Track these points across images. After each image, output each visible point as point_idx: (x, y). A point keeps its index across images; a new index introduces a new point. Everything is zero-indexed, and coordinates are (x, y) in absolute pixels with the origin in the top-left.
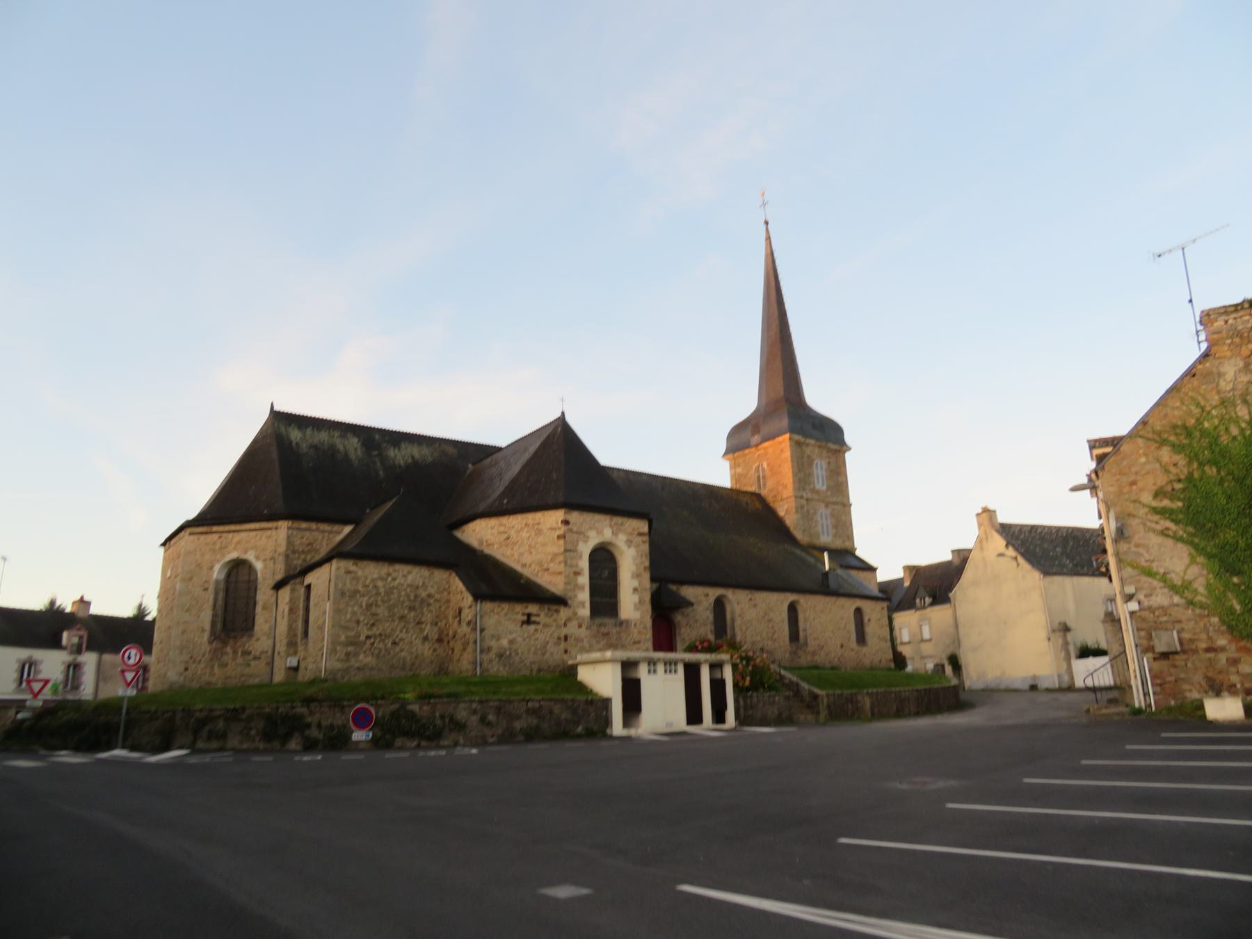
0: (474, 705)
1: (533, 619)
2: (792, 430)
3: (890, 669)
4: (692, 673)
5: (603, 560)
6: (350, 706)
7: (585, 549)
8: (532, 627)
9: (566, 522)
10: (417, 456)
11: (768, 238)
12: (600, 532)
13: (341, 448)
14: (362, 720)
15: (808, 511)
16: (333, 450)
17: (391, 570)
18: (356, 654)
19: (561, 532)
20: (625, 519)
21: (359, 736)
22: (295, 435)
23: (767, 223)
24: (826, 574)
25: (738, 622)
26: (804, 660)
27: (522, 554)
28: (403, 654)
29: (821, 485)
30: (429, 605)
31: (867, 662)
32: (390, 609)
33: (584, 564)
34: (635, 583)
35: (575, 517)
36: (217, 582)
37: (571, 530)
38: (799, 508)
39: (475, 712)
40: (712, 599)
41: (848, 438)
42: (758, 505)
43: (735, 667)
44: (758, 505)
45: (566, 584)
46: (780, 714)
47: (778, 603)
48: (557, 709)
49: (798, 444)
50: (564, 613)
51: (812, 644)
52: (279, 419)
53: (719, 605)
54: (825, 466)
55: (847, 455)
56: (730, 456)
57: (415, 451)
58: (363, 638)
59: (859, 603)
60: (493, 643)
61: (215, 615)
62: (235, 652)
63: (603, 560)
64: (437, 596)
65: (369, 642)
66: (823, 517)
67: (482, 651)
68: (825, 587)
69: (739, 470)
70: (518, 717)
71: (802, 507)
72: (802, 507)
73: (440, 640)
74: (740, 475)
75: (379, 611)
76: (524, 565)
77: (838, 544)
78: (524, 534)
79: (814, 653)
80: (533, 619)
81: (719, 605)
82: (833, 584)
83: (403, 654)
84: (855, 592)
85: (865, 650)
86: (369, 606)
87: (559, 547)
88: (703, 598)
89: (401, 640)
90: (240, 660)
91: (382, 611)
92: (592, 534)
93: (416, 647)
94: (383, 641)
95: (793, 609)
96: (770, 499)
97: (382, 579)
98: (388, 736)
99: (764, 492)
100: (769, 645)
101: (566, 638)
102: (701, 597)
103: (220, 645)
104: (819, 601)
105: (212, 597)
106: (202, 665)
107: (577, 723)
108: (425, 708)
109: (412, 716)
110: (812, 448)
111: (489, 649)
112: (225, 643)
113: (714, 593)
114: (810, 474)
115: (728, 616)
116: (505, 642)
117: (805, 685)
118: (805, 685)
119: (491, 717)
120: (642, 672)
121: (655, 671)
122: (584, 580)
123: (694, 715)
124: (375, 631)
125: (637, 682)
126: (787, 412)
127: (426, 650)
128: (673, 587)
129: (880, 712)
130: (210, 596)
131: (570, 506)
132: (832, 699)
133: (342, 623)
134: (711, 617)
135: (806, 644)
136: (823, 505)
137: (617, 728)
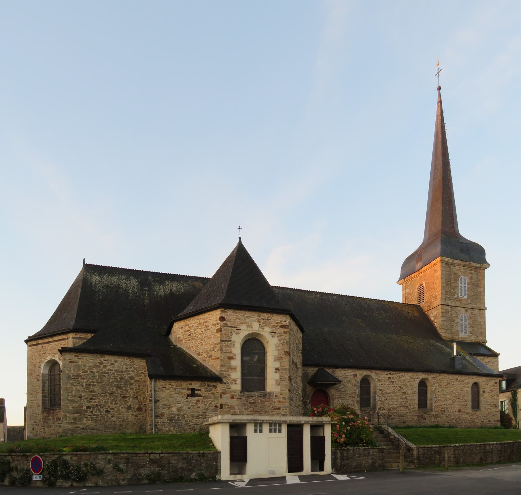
0: (109, 457)
1: (196, 392)
2: (443, 254)
3: (496, 428)
4: (295, 434)
5: (253, 346)
6: (31, 456)
7: (238, 340)
8: (196, 398)
9: (222, 319)
10: (174, 289)
11: (440, 102)
12: (249, 326)
13: (124, 286)
14: (37, 466)
15: (452, 315)
16: (118, 287)
17: (102, 359)
18: (81, 419)
19: (218, 327)
20: (270, 315)
21: (36, 477)
22: (96, 279)
23: (439, 88)
24: (454, 358)
25: (379, 394)
26: (429, 421)
27: (197, 346)
28: (114, 419)
29: (463, 295)
30: (131, 384)
31: (478, 422)
32: (102, 388)
33: (237, 351)
34: (277, 365)
35: (230, 314)
36: (44, 375)
37: (226, 325)
38: (445, 314)
39: (110, 462)
40: (359, 378)
41: (488, 258)
42: (416, 314)
43: (333, 426)
44: (416, 314)
45: (222, 366)
46: (374, 463)
47: (410, 381)
48: (174, 460)
49: (448, 264)
50: (220, 388)
51: (436, 410)
52: (89, 269)
53: (365, 383)
54: (467, 280)
55: (487, 272)
56: (402, 281)
57: (174, 286)
58: (84, 408)
59: (476, 379)
60: (166, 411)
61: (44, 396)
62: (54, 419)
63: (253, 346)
64: (137, 378)
65: (89, 410)
66: (463, 318)
67: (156, 416)
68: (452, 368)
69: (408, 290)
70: (143, 466)
71: (447, 312)
72: (447, 312)
73: (139, 409)
74: (408, 294)
75: (95, 389)
76: (198, 354)
77: (473, 339)
78: (199, 331)
79: (436, 416)
80: (196, 392)
81: (365, 383)
82: (458, 366)
83: (114, 419)
84: (476, 371)
85: (478, 413)
86: (88, 385)
87: (216, 339)
88: (352, 378)
89: (112, 409)
90: (56, 424)
91: (97, 389)
92: (243, 327)
93: (122, 414)
94: (99, 410)
95: (423, 385)
96: (425, 309)
97: (96, 366)
98: (52, 479)
99: (422, 305)
100: (403, 411)
101: (221, 406)
102: (349, 378)
103: (47, 415)
104: (444, 378)
105: (41, 385)
106: (40, 426)
107: (191, 471)
108: (75, 458)
109: (65, 464)
110: (458, 266)
111: (163, 415)
112: (49, 413)
113: (361, 374)
114: (456, 287)
115: (372, 390)
116: (174, 410)
117: (404, 440)
118: (404, 440)
119: (121, 466)
120: (250, 431)
121: (261, 431)
122: (237, 363)
123: (295, 463)
124: (93, 403)
125: (244, 439)
126: (451, 249)
127: (130, 416)
128: (329, 371)
129: (459, 463)
130: (40, 383)
131: (225, 306)
132: (422, 451)
133: (70, 398)
134: (358, 391)
135: (431, 410)
136: (463, 310)
137: (225, 473)
